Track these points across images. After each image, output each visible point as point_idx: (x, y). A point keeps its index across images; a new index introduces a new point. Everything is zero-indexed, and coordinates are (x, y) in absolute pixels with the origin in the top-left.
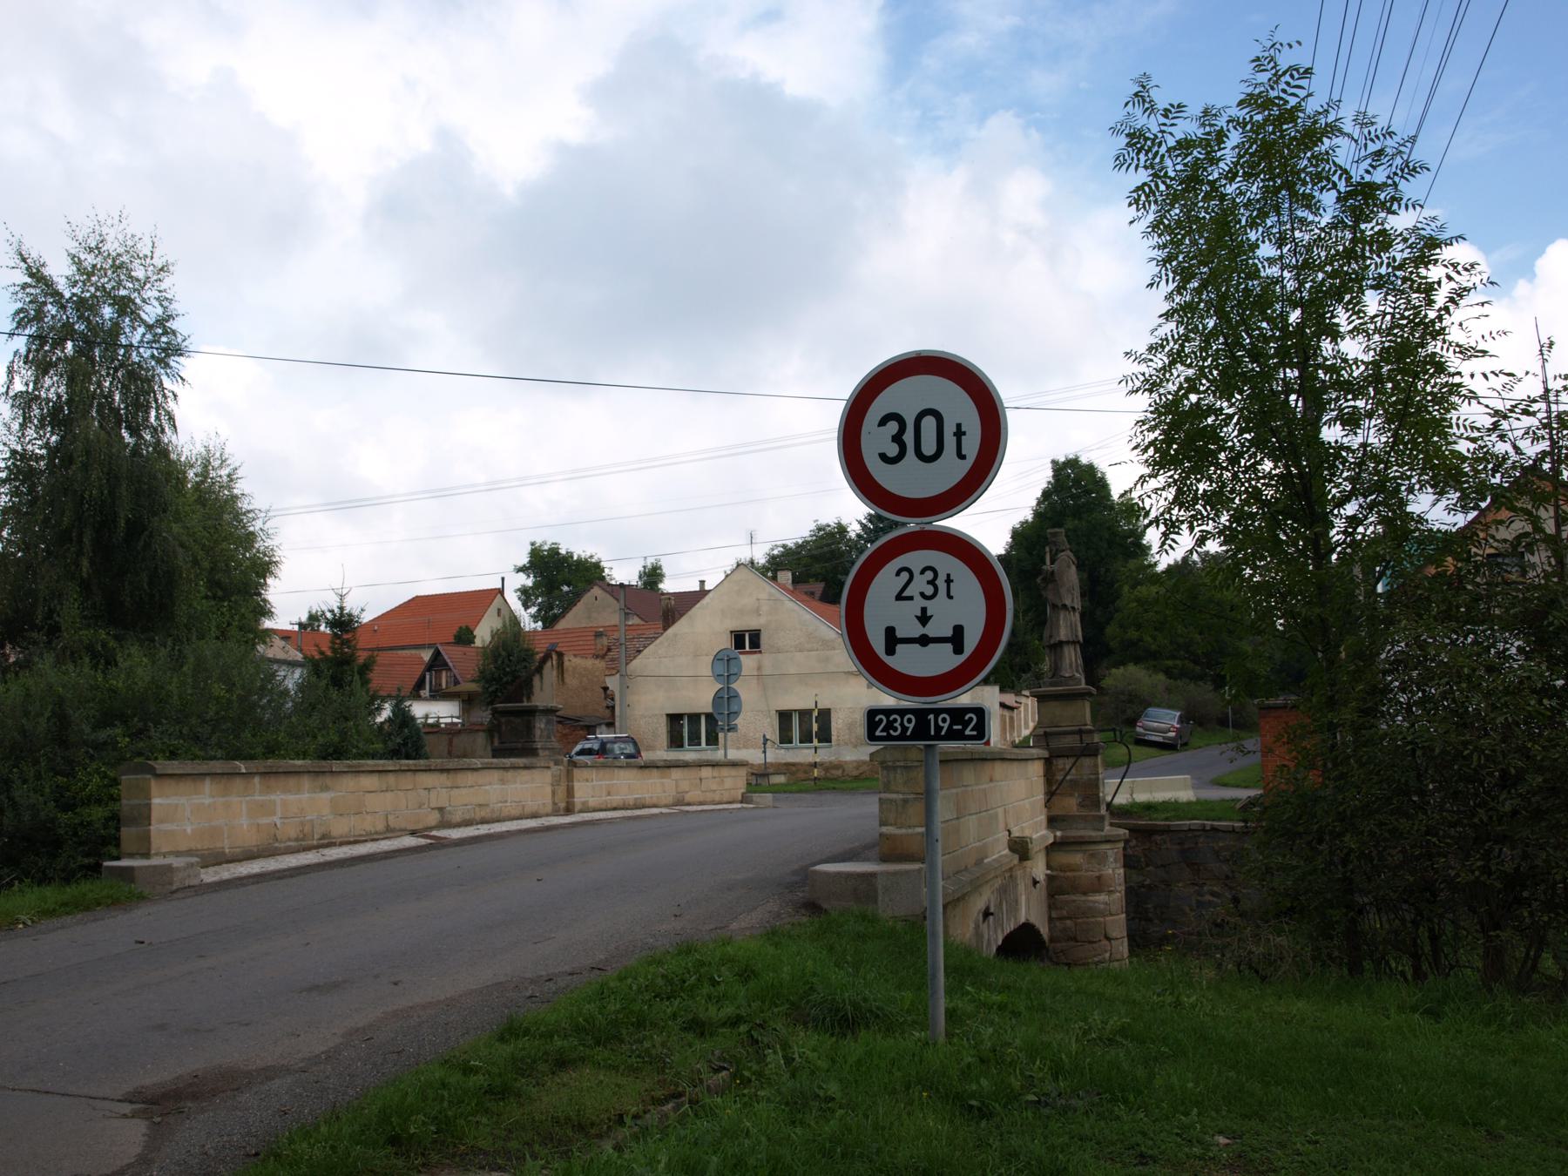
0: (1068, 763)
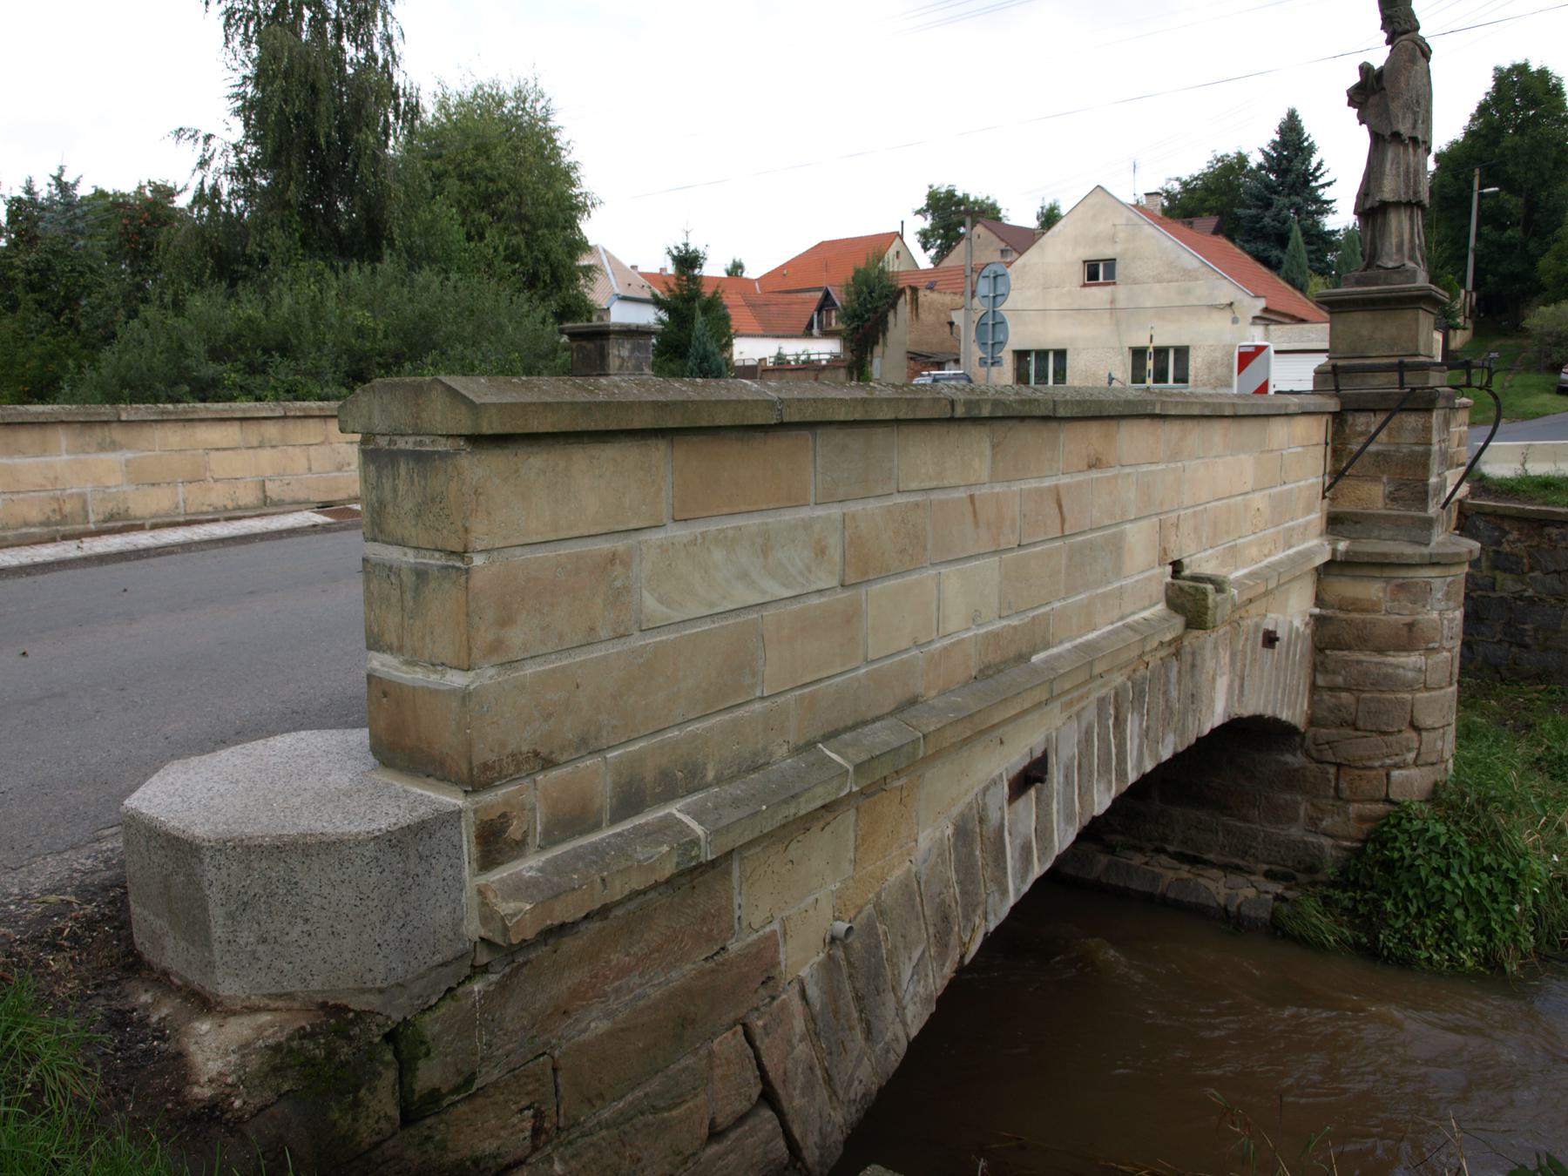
0: (1372, 422)
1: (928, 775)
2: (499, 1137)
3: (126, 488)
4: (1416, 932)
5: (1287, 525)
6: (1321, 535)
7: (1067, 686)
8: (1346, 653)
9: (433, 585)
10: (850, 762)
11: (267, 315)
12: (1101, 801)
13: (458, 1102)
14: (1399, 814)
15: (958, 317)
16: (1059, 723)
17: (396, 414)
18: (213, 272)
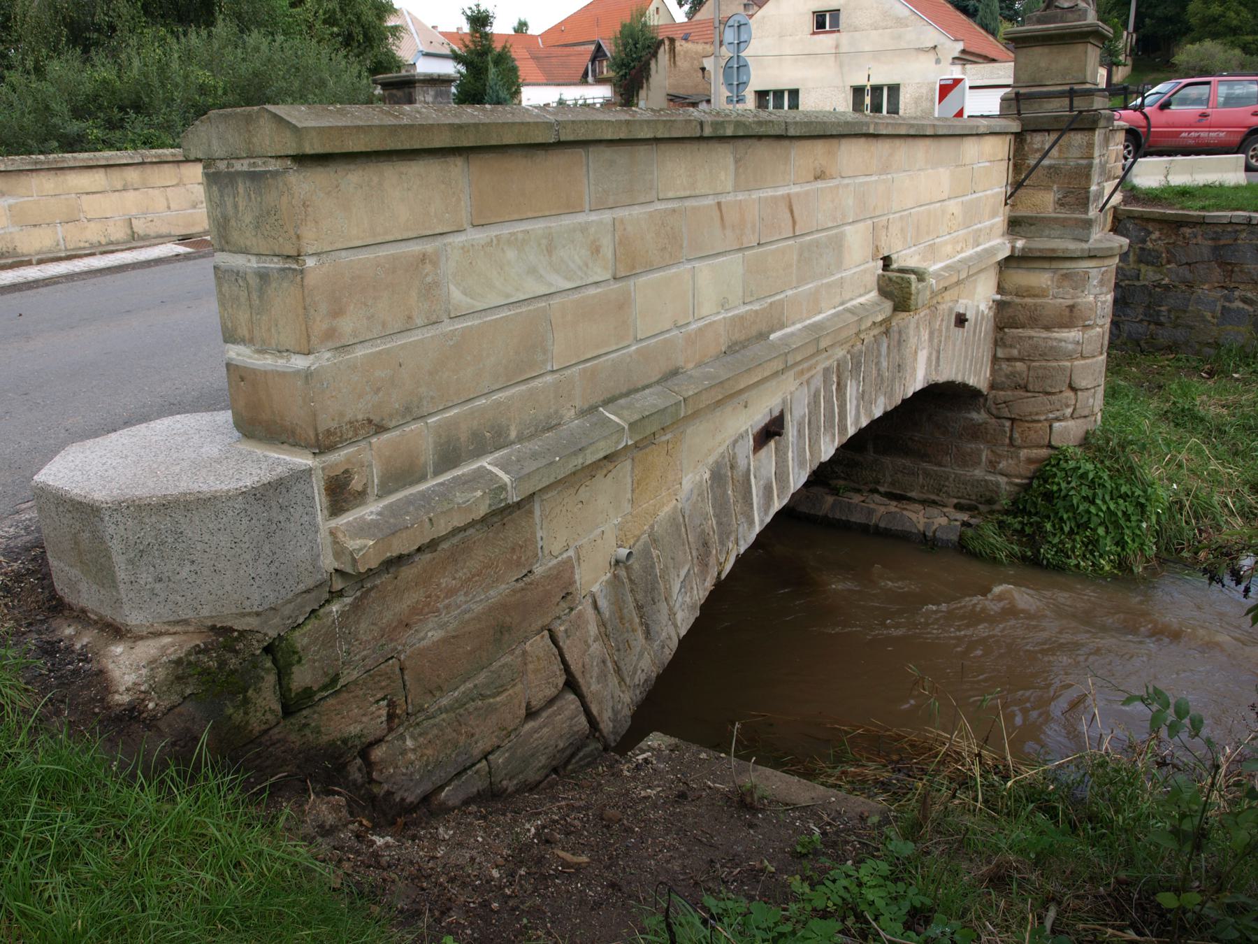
0: (1047, 140)
1: (689, 431)
2: (361, 722)
3: (12, 230)
4: (1068, 546)
5: (975, 227)
7: (799, 358)
8: (1020, 330)
9: (274, 285)
11: (119, 77)
12: (827, 451)
13: (327, 696)
14: (1058, 456)
15: (708, 64)
16: (793, 389)
17: (231, 140)
18: (68, 40)
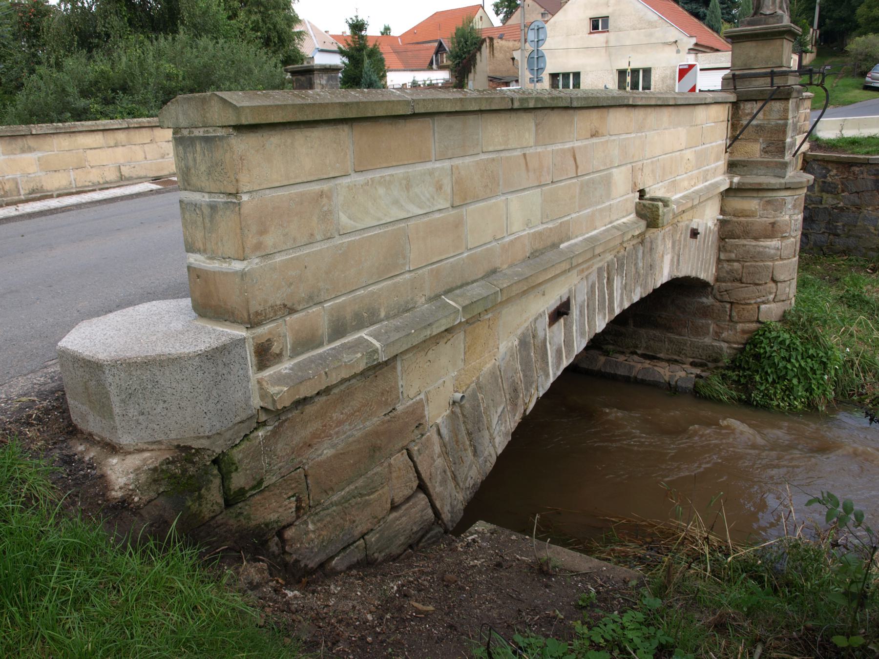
0: (756, 106)
1: (504, 312)
2: (278, 512)
3: (40, 174)
6: (724, 174)
7: (580, 261)
8: (737, 240)
9: (220, 213)
10: (460, 305)
12: (600, 325)
13: (255, 494)
14: (765, 328)
15: (517, 55)
16: (576, 282)
17: (192, 115)
